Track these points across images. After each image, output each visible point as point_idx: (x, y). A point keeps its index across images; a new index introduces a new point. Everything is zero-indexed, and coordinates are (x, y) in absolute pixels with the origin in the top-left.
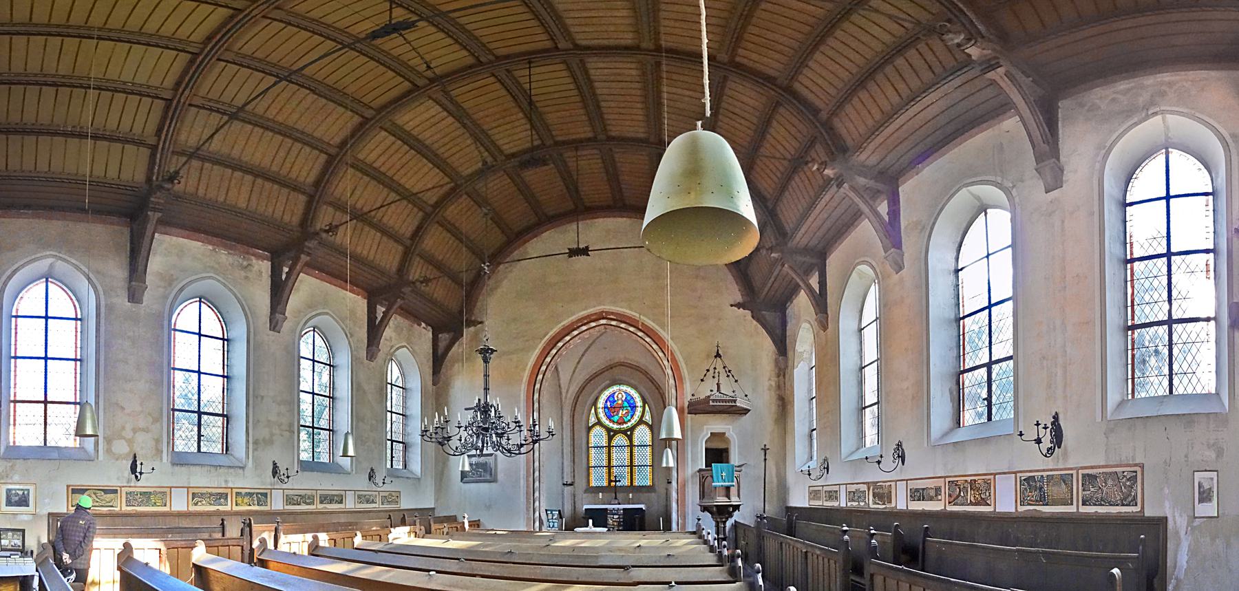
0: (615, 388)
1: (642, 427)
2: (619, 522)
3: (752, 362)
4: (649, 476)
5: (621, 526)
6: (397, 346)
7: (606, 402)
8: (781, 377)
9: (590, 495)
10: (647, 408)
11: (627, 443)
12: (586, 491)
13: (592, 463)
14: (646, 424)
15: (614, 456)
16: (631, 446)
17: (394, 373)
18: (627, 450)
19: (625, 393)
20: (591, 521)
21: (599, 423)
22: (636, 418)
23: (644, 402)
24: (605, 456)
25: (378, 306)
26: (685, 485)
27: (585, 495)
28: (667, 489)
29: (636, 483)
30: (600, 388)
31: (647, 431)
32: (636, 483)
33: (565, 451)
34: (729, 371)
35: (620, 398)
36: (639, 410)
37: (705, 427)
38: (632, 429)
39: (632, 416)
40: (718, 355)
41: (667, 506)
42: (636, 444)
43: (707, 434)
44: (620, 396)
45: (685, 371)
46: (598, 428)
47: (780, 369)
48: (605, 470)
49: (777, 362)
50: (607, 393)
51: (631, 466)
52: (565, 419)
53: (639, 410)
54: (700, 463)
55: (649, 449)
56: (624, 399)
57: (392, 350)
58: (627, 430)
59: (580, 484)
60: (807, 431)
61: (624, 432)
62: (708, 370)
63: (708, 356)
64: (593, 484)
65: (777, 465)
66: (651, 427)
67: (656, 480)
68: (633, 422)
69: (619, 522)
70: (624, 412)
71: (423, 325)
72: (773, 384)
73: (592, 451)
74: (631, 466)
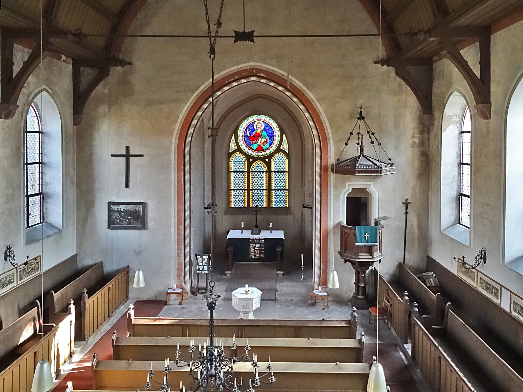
0: (255, 118)
1: (280, 155)
2: (260, 250)
3: (395, 120)
4: (286, 199)
5: (262, 254)
6: (36, 91)
7: (246, 130)
8: (425, 134)
9: (229, 216)
10: (284, 137)
11: (265, 169)
12: (225, 213)
13: (232, 186)
14: (284, 152)
15: (252, 180)
16: (269, 172)
17: (32, 123)
18: (265, 175)
19: (264, 122)
20: (234, 335)
21: (239, 150)
22: (274, 146)
23: (282, 131)
24: (245, 181)
25: (15, 45)
26: (327, 235)
27: (224, 217)
28: (302, 213)
29: (273, 205)
30: (240, 118)
31: (284, 158)
32: (273, 205)
33: (206, 176)
34: (373, 134)
35: (259, 128)
36: (277, 139)
37: (347, 183)
38: (270, 156)
39: (270, 145)
40: (361, 118)
41: (302, 226)
42: (274, 170)
43: (349, 190)
44: (259, 125)
45: (330, 131)
46: (238, 154)
47: (424, 126)
48: (244, 193)
49: (421, 120)
50: (247, 122)
51: (269, 190)
52: (206, 146)
53: (276, 142)
54: (341, 215)
55: (286, 175)
56: (263, 128)
57: (30, 99)
58: (266, 157)
59: (221, 207)
60: (454, 193)
61: (263, 159)
62: (352, 134)
63: (351, 117)
64: (233, 205)
65: (419, 217)
66: (288, 155)
67: (292, 201)
68: (271, 150)
69: (260, 250)
70: (263, 140)
71: (63, 57)
72: (417, 140)
73: (232, 175)
74: (269, 190)
